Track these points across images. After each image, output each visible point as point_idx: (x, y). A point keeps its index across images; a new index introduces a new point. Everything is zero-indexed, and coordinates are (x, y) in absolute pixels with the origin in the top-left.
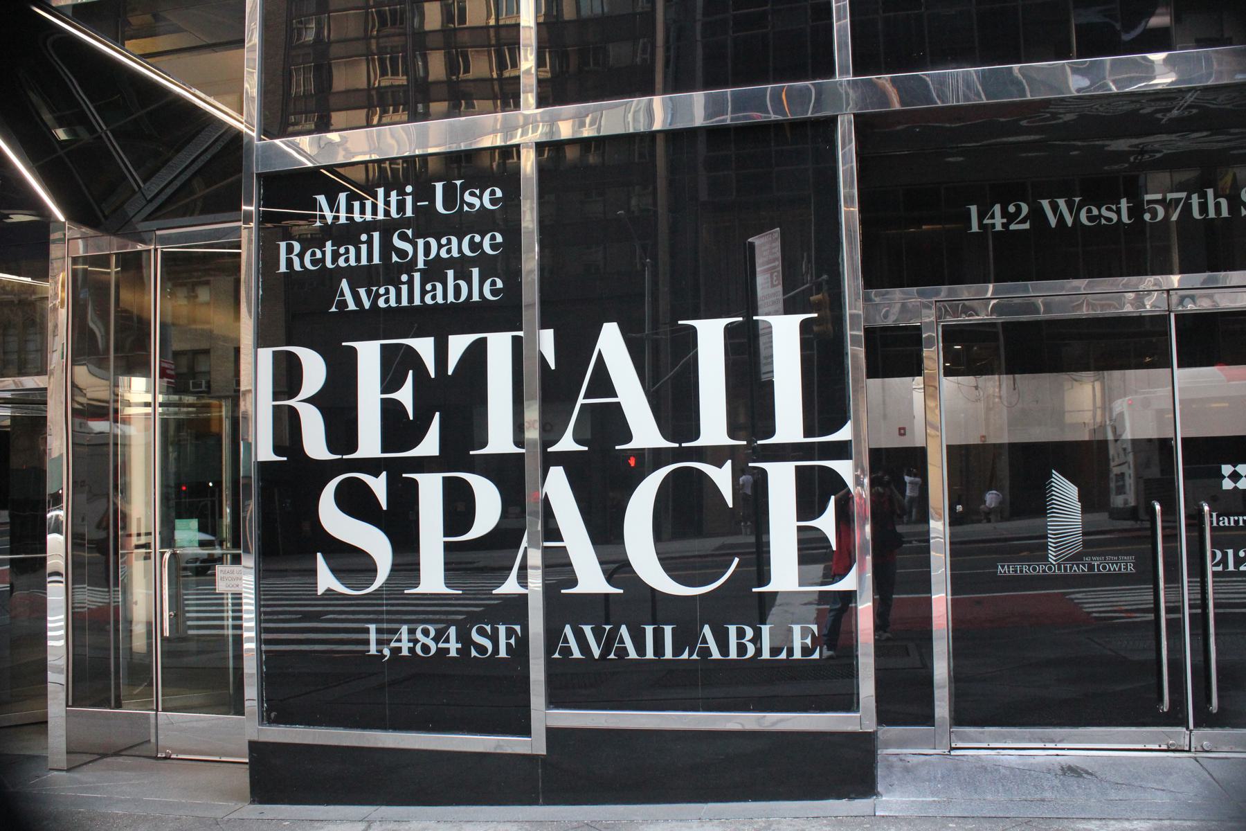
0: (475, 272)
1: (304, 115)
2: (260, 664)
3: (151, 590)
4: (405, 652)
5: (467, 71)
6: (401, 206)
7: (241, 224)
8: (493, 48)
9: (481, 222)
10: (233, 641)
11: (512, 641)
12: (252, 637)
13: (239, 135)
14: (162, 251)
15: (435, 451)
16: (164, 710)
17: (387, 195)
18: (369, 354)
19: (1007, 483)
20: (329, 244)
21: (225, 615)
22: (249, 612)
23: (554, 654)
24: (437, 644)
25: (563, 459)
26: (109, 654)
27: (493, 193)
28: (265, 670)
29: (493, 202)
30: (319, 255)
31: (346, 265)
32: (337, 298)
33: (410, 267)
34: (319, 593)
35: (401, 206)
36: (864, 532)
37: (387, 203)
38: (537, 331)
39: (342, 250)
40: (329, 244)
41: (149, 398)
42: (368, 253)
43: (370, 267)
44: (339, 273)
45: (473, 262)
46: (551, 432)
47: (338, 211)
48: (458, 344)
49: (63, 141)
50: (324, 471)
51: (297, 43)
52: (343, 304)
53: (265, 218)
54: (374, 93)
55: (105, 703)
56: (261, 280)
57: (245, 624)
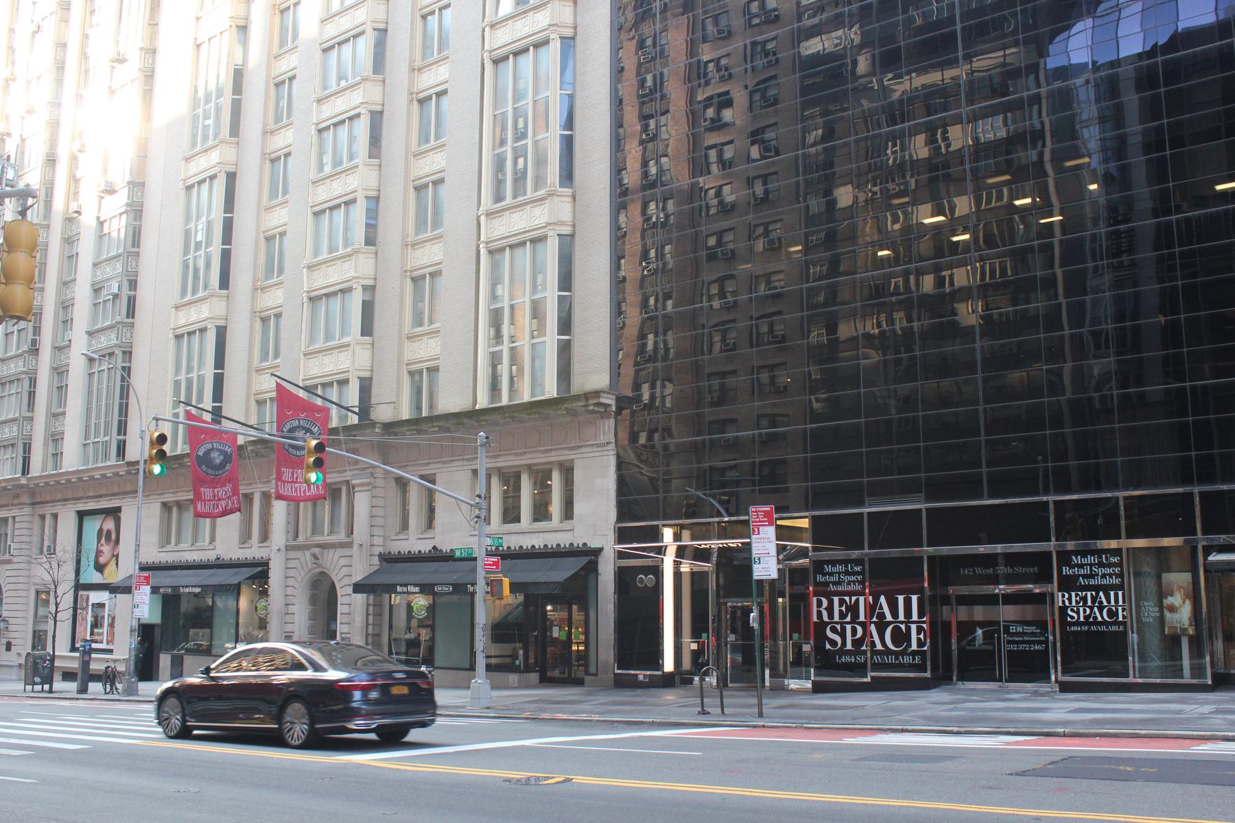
6: (1094, 560)
9: (1115, 565)
18: (836, 599)
19: (740, 631)
25: (874, 622)
35: (1094, 560)
42: (1087, 571)
44: (1079, 575)
48: (854, 598)
50: (828, 623)
52: (1080, 583)
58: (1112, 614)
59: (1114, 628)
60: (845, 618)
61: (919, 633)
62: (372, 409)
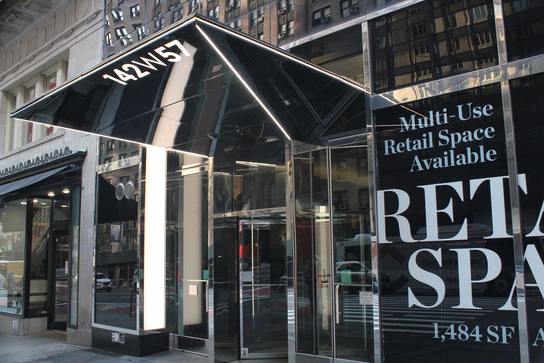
0: (482, 148)
1: (382, 81)
2: (382, 339)
3: (331, 300)
4: (453, 338)
5: (458, 48)
7: (366, 133)
8: (470, 35)
9: (483, 122)
10: (367, 325)
11: (510, 335)
12: (378, 324)
13: (363, 93)
14: (331, 149)
15: (465, 237)
16: (336, 357)
17: (434, 114)
20: (408, 140)
21: (363, 313)
22: (376, 312)
23: (534, 343)
24: (469, 335)
25: (535, 241)
26: (313, 329)
27: (488, 107)
28: (384, 342)
29: (488, 112)
30: (403, 145)
31: (417, 149)
32: (413, 165)
33: (448, 147)
34: (410, 306)
37: (435, 118)
38: (516, 175)
39: (414, 142)
40: (408, 140)
41: (328, 215)
43: (429, 149)
44: (414, 153)
45: (479, 143)
46: (527, 225)
47: (411, 124)
48: (475, 184)
49: (288, 105)
50: (412, 247)
51: (377, 49)
52: (416, 168)
53: (377, 130)
54: (413, 66)
55: (311, 352)
56: (377, 159)
57: (374, 318)
60: (456, 233)
62: (18, 24)
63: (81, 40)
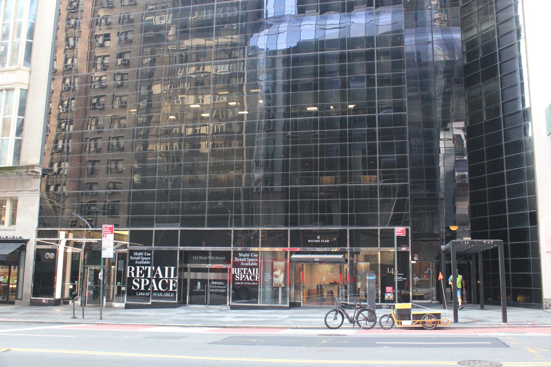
9: (256, 258)
18: (138, 268)
36: (177, 286)
44: (136, 260)
48: (146, 267)
50: (135, 278)
58: (253, 278)
59: (254, 283)
61: (173, 283)
63: (526, 47)
